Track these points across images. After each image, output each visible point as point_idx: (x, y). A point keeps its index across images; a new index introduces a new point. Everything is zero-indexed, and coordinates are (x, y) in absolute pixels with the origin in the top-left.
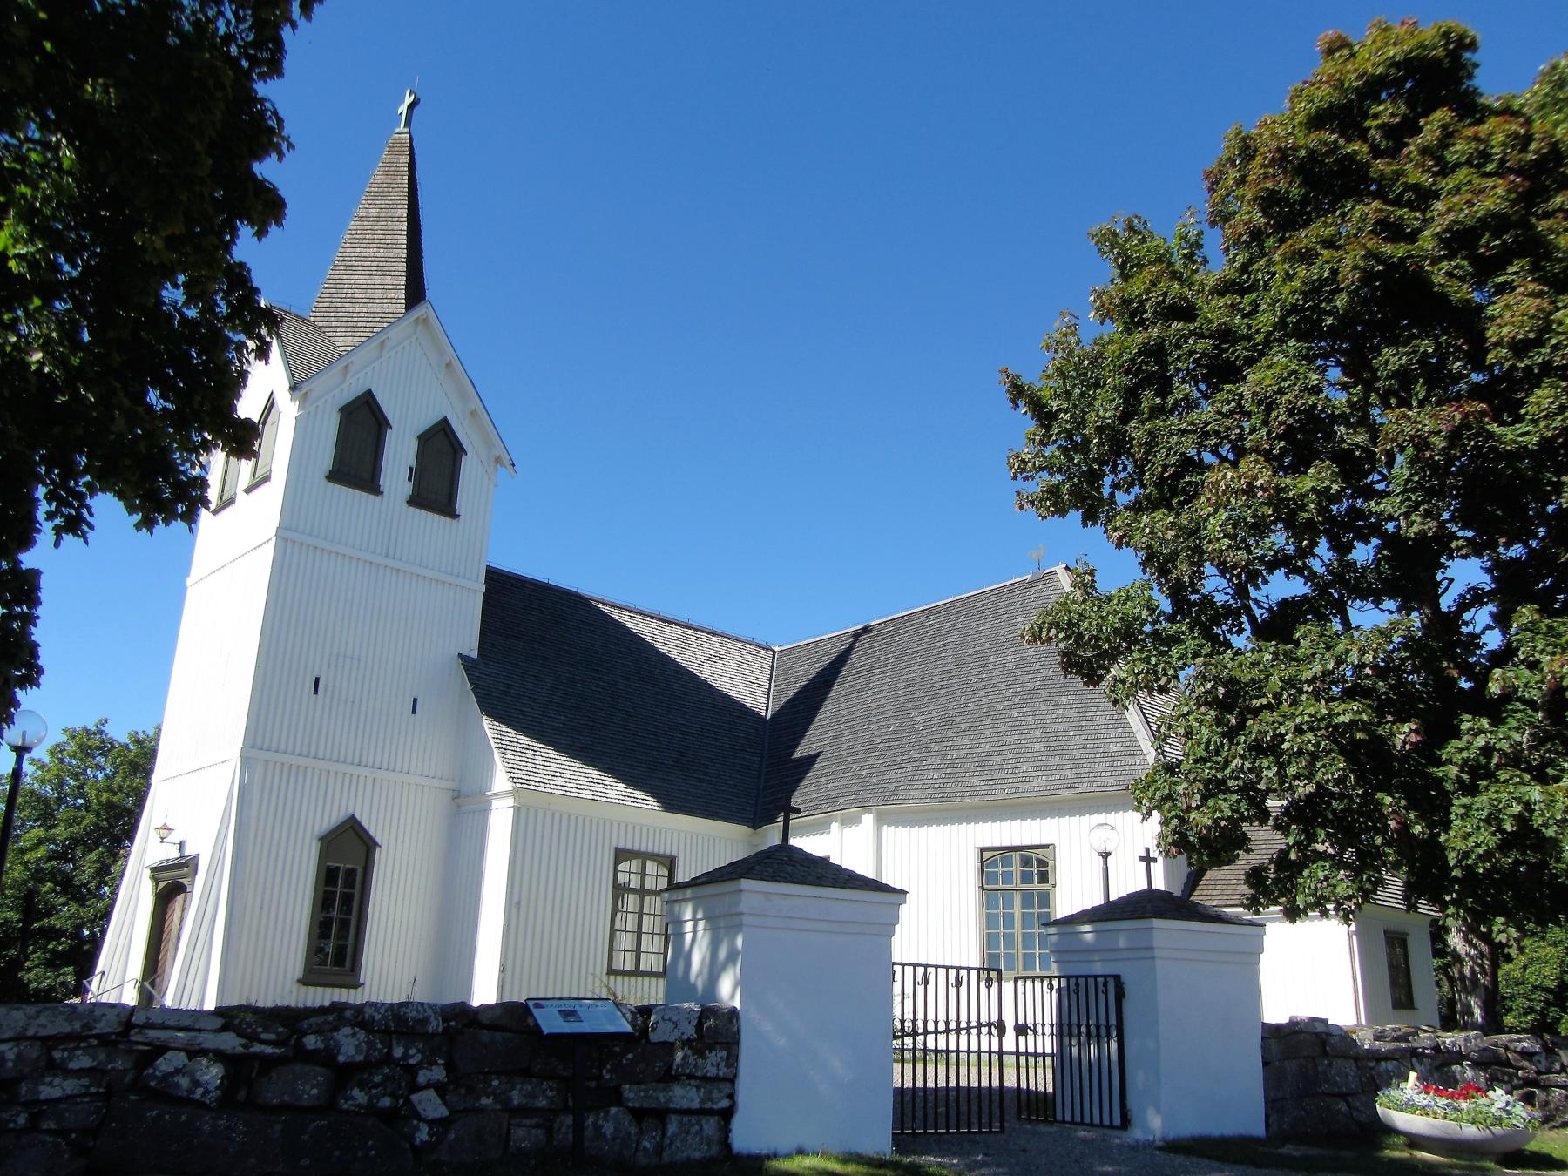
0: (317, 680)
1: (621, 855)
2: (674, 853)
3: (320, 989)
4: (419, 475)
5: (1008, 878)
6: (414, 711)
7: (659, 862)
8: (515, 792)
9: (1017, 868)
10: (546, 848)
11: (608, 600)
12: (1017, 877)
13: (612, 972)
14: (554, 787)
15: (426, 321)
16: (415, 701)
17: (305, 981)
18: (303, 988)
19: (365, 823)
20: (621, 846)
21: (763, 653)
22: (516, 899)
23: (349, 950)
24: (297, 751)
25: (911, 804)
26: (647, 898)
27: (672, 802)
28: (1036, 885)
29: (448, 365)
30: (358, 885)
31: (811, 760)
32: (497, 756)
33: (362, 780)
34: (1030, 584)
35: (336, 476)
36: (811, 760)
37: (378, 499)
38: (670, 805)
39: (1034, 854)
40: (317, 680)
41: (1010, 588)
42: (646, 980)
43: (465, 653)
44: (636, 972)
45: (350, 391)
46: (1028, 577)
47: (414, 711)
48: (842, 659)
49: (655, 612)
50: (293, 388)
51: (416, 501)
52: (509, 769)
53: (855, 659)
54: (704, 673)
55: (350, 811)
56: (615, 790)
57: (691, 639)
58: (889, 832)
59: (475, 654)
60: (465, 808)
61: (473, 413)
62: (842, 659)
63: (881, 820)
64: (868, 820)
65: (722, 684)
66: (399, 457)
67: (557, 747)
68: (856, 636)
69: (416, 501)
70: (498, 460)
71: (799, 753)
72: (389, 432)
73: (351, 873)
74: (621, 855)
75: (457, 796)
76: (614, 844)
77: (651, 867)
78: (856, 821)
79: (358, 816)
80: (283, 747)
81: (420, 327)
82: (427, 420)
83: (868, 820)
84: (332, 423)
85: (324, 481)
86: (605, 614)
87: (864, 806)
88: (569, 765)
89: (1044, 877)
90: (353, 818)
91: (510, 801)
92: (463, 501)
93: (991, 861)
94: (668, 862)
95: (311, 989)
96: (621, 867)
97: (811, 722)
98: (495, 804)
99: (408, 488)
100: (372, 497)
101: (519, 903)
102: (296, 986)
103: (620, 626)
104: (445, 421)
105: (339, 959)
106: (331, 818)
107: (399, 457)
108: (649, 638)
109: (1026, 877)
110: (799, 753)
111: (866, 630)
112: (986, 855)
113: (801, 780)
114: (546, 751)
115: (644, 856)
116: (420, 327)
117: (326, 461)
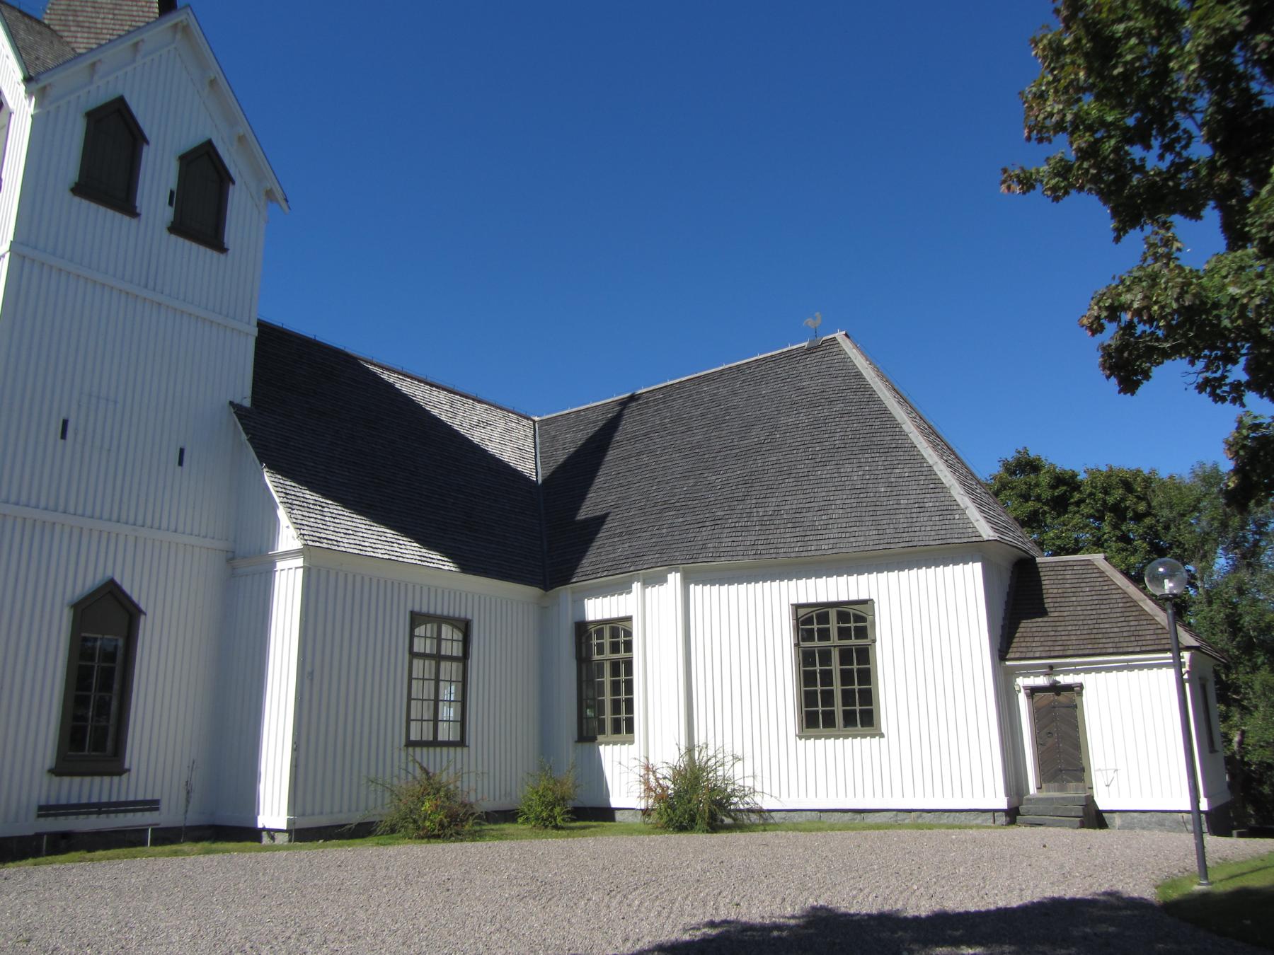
0: (65, 423)
1: (417, 619)
2: (469, 617)
3: (77, 779)
4: (179, 199)
5: (824, 635)
6: (181, 463)
7: (454, 626)
8: (306, 551)
9: (833, 626)
10: (394, 624)
11: (375, 361)
12: (834, 633)
13: (410, 744)
14: (347, 545)
15: (186, 29)
16: (182, 451)
17: (60, 769)
18: (56, 779)
19: (126, 587)
20: (417, 609)
21: (524, 422)
22: (308, 668)
23: (112, 730)
24: (43, 504)
25: (723, 562)
26: (443, 664)
27: (470, 562)
28: (816, 643)
29: (213, 83)
30: (116, 686)
31: (599, 521)
32: (282, 513)
33: (122, 538)
34: (810, 350)
35: (81, 189)
36: (599, 521)
37: (134, 221)
38: (466, 566)
39: (852, 610)
40: (65, 423)
41: (788, 356)
42: (445, 749)
43: (237, 401)
44: (435, 743)
45: (100, 93)
46: (805, 344)
47: (181, 463)
48: (611, 426)
49: (422, 377)
50: (28, 80)
51: (178, 228)
52: (298, 526)
53: (627, 426)
54: (476, 436)
55: (109, 573)
56: (410, 551)
57: (459, 404)
58: (696, 590)
59: (247, 403)
60: (246, 572)
61: (242, 139)
62: (611, 426)
63: (687, 581)
64: (674, 579)
65: (493, 448)
66: (158, 177)
67: (346, 504)
68: (624, 404)
69: (178, 228)
70: (269, 195)
71: (582, 515)
72: (145, 148)
73: (110, 656)
74: (417, 619)
75: (231, 558)
76: (409, 608)
77: (446, 631)
78: (662, 580)
79: (118, 579)
80: (24, 499)
81: (179, 36)
82: (190, 141)
83: (674, 579)
84: (76, 132)
85: (69, 195)
86: (375, 374)
87: (673, 567)
88: (360, 524)
89: (862, 633)
90: (112, 582)
91: (299, 562)
92: (233, 232)
93: (811, 623)
94: (462, 626)
95: (66, 779)
96: (417, 632)
97: (590, 485)
98: (280, 565)
99: (168, 214)
100: (126, 219)
101: (312, 673)
102: (46, 778)
103: (391, 386)
104: (209, 143)
105: (99, 745)
106: (87, 581)
107: (158, 177)
108: (419, 400)
109: (844, 634)
110: (582, 515)
111: (633, 398)
112: (802, 612)
113: (591, 540)
114: (333, 508)
115: (439, 620)
116: (179, 36)
117: (71, 171)
